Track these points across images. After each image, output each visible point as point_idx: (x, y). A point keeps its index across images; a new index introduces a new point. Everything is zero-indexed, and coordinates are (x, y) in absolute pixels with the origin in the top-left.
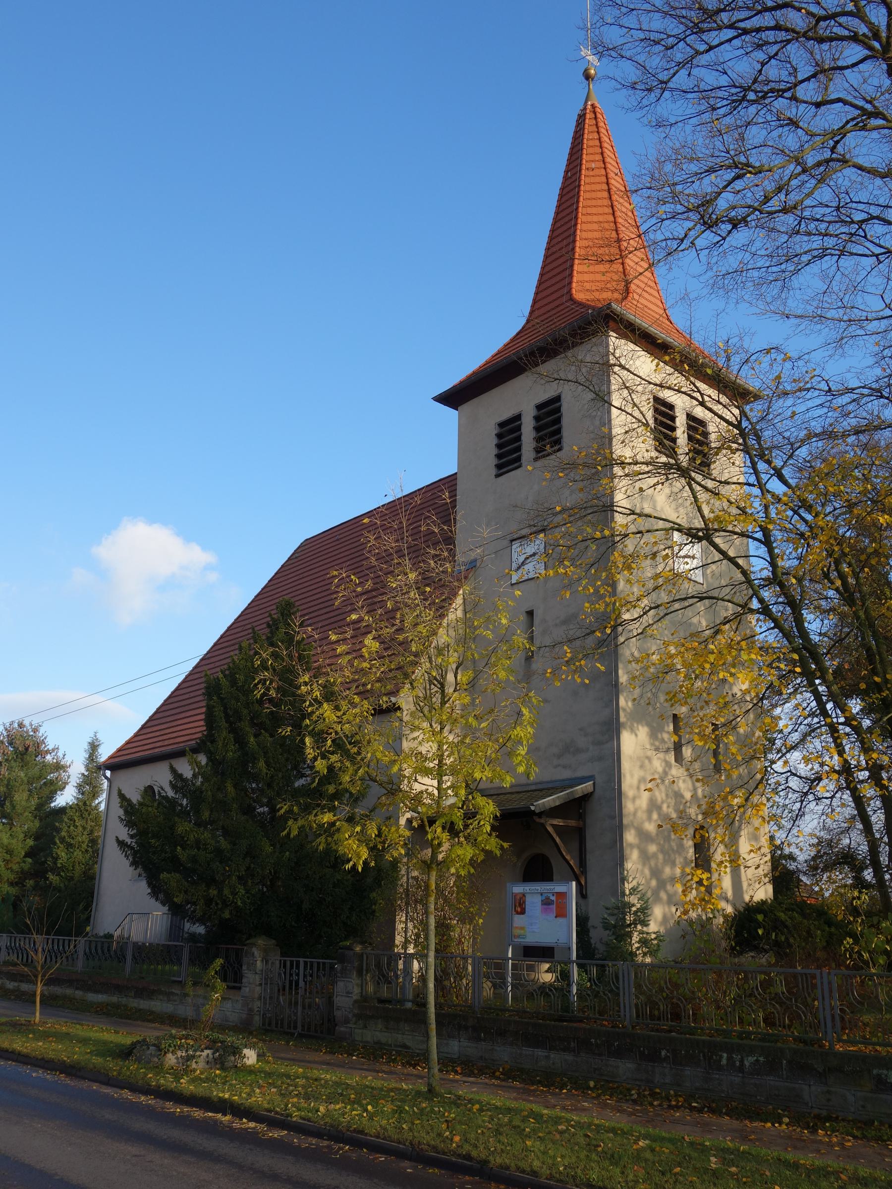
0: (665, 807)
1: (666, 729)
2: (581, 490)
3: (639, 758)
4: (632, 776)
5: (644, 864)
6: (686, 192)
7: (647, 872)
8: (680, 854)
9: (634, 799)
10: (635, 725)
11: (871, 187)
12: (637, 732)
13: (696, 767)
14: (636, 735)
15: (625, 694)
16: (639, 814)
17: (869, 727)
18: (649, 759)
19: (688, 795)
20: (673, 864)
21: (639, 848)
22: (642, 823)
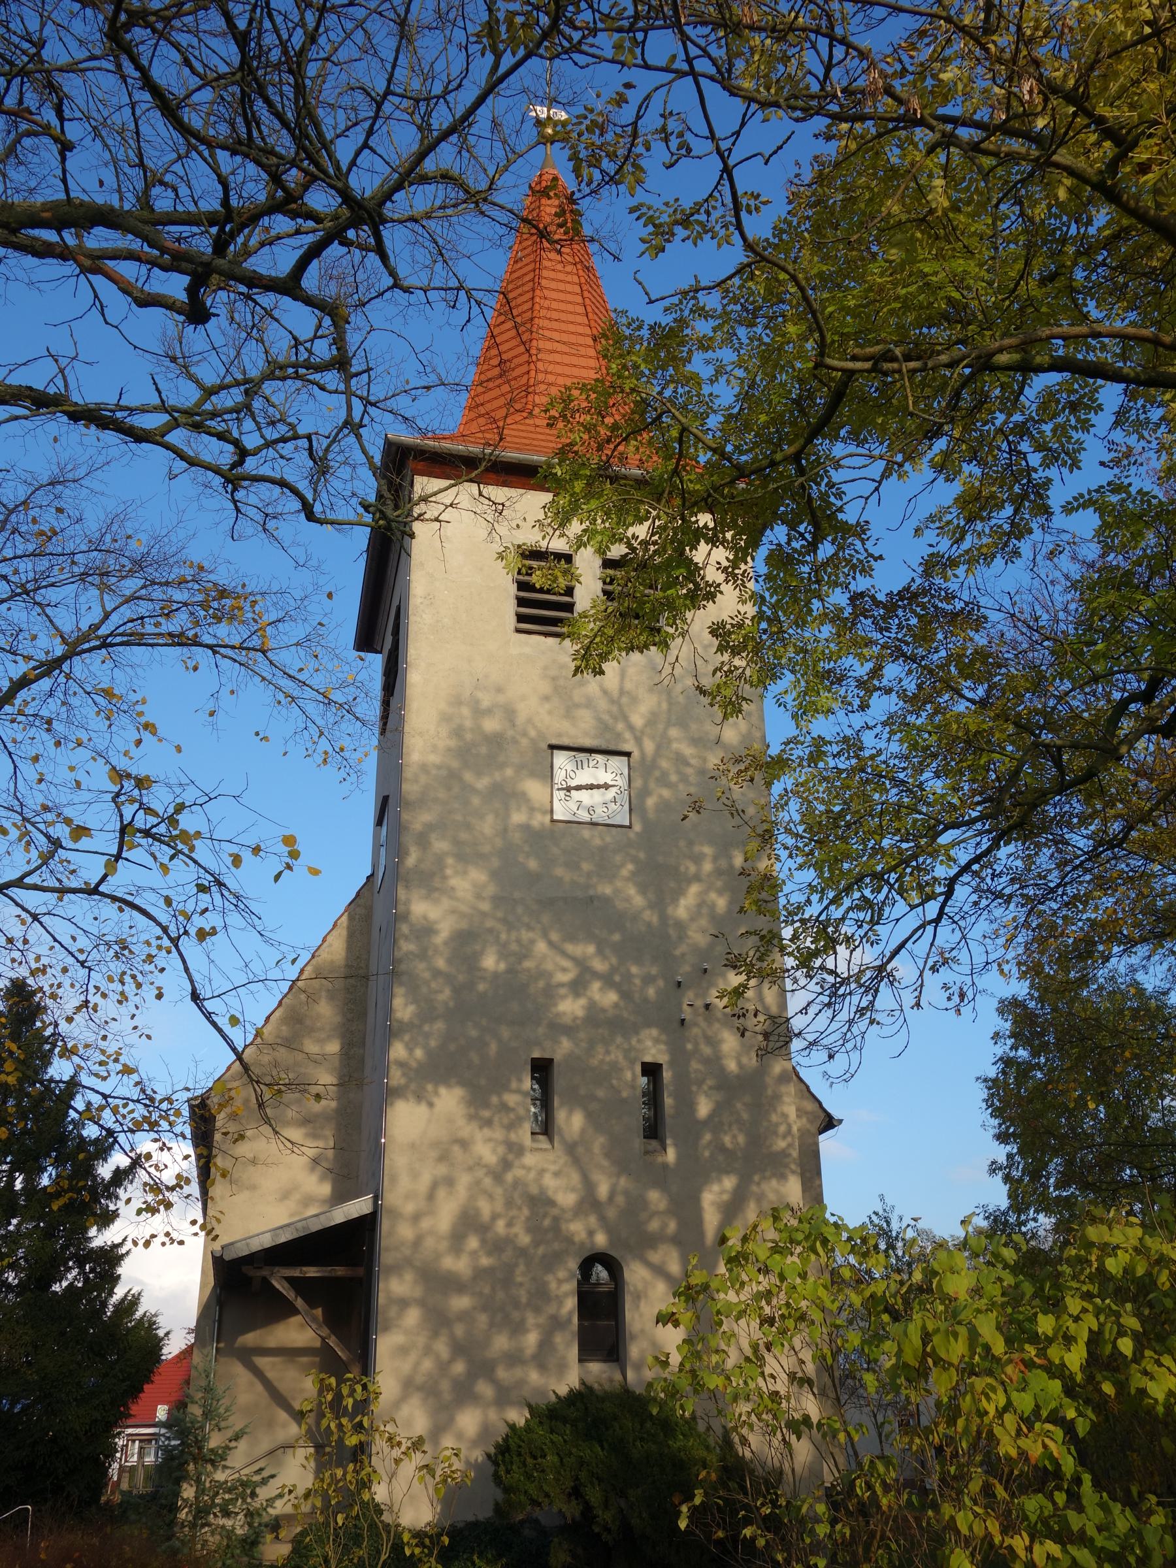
0: (500, 1226)
1: (514, 1085)
2: (139, 986)
3: (435, 1144)
4: (415, 1175)
5: (435, 1334)
6: (900, 1253)
7: (442, 1348)
8: (537, 1310)
9: (416, 1218)
10: (430, 1087)
11: (617, 417)
12: (435, 1100)
13: (577, 490)
14: (431, 1105)
15: (407, 1037)
16: (429, 1243)
17: (1056, 1229)
18: (464, 1144)
19: (567, 1199)
20: (518, 1329)
21: (422, 1303)
22: (438, 1256)
